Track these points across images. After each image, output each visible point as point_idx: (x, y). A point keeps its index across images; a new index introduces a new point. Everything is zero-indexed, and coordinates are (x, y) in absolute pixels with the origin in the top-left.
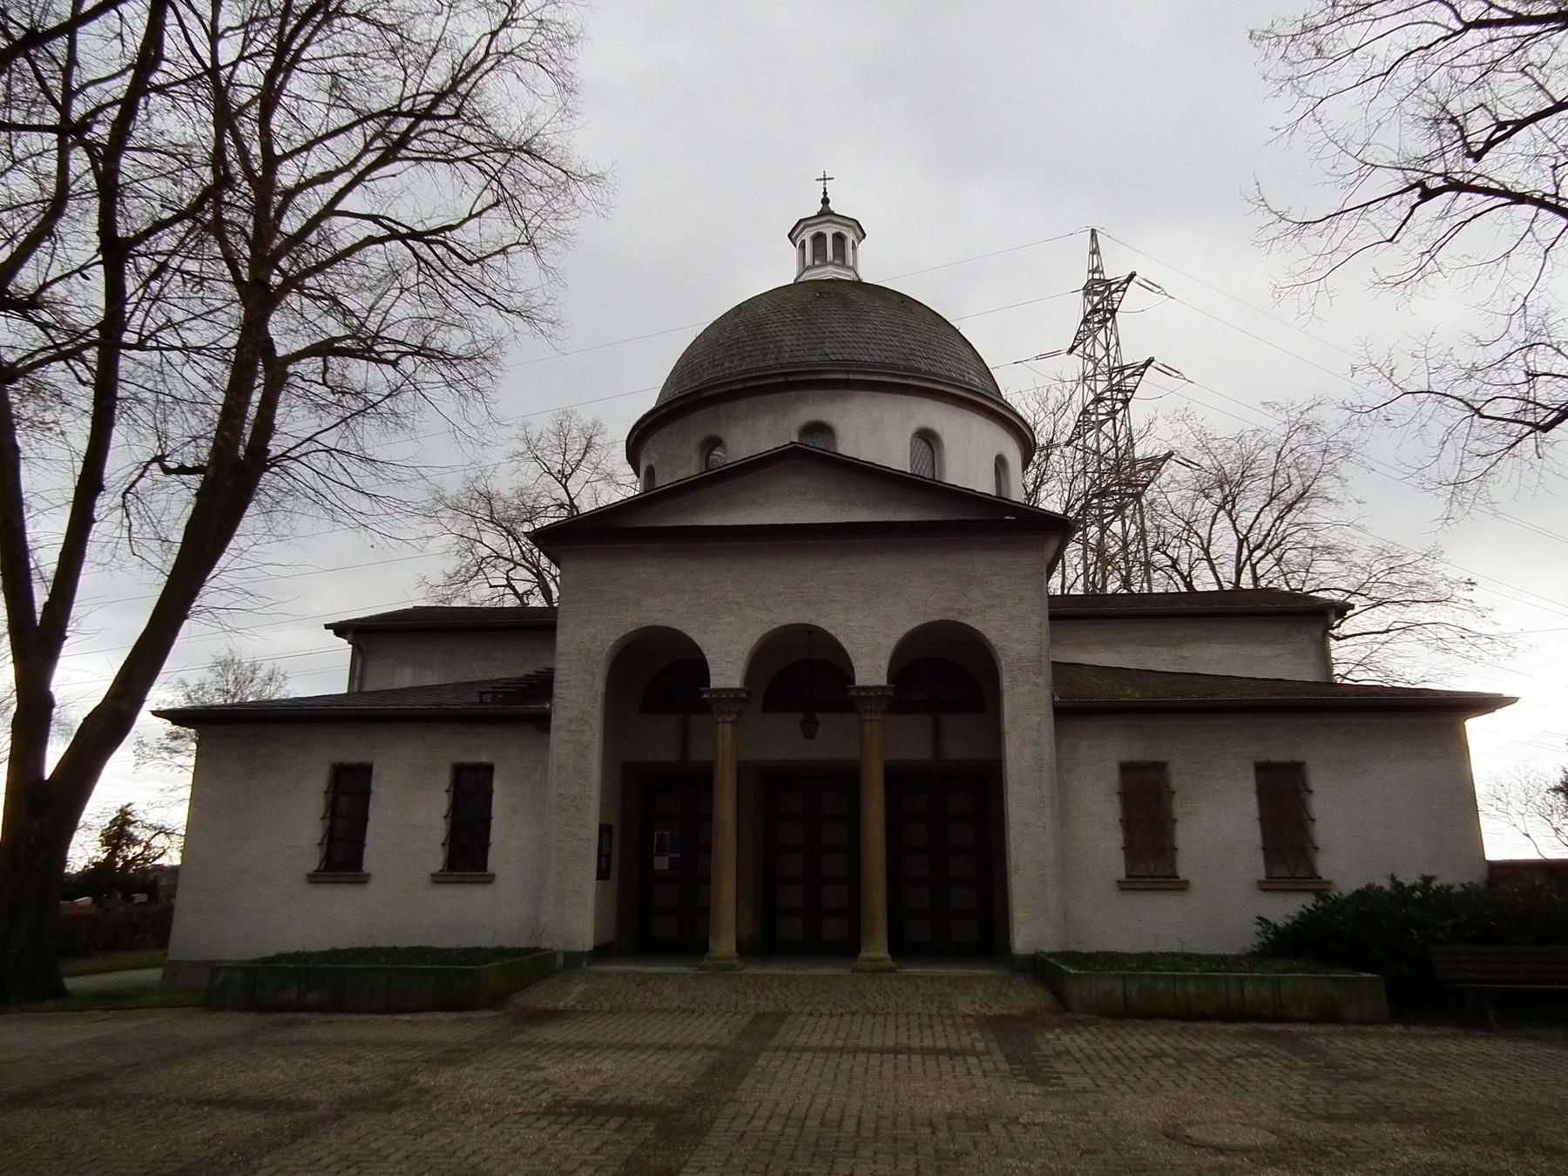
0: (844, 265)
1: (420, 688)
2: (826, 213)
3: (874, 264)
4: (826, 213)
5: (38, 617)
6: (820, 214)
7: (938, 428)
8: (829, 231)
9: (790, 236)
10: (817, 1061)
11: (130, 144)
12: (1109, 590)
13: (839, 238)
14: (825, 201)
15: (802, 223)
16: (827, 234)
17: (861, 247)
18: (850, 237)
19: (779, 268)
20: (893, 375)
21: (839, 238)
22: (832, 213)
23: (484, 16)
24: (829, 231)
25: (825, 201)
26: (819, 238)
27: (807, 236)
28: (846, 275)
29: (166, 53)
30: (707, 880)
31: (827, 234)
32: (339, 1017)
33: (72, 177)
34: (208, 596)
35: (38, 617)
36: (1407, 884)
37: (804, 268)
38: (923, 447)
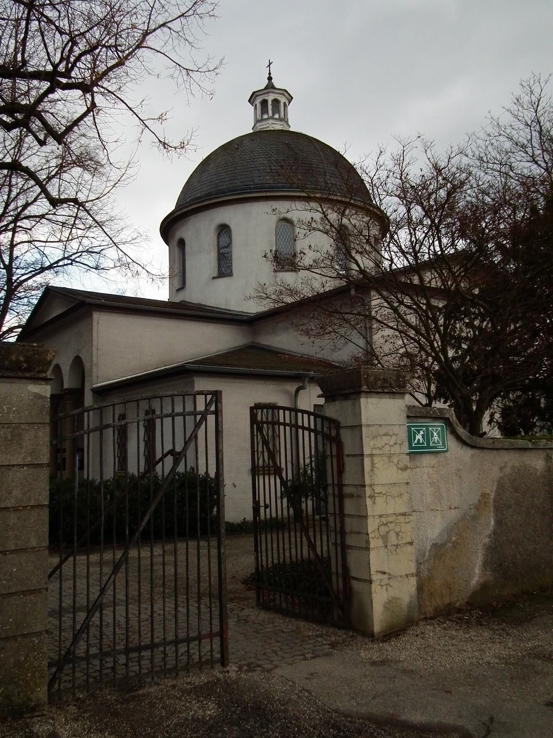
2: (270, 86)
3: (300, 120)
4: (270, 86)
6: (266, 88)
7: (227, 222)
8: (270, 98)
10: (161, 635)
12: (32, 102)
14: (270, 79)
16: (269, 100)
17: (290, 108)
18: (283, 100)
19: (241, 122)
20: (233, 195)
21: (276, 102)
23: (55, 180)
24: (270, 98)
25: (270, 79)
26: (264, 103)
29: (46, 200)
31: (269, 100)
32: (95, 343)
34: (197, 404)
36: (252, 570)
37: (257, 121)
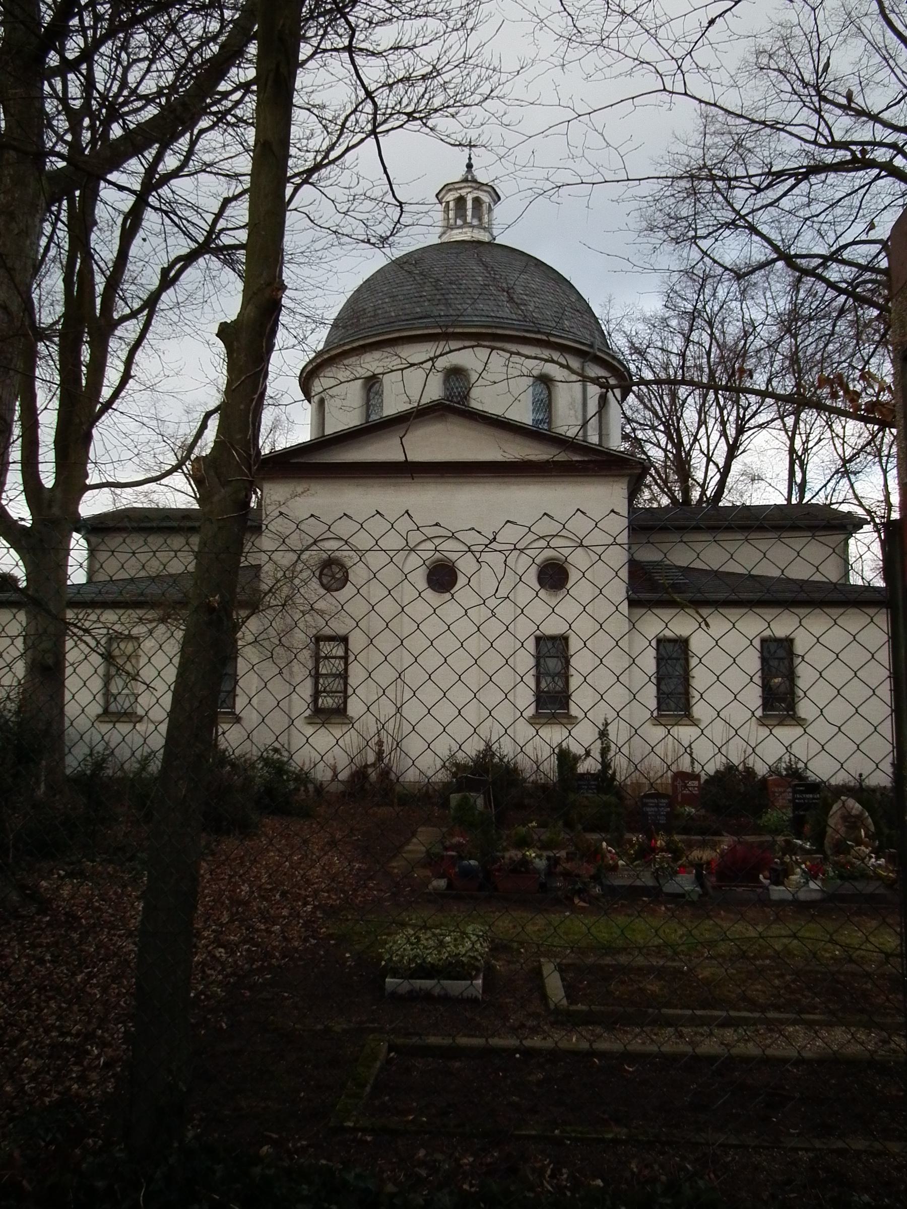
0: (480, 227)
1: (569, 282)
2: (469, 180)
4: (469, 180)
5: (98, 311)
6: (466, 180)
9: (437, 196)
11: (289, 173)
13: (477, 201)
14: (469, 166)
15: (448, 188)
17: (498, 210)
22: (475, 181)
25: (469, 166)
26: (461, 201)
27: (451, 197)
28: (484, 237)
30: (442, 477)
33: (748, 396)
35: (98, 311)
37: (449, 227)
38: (541, 388)
